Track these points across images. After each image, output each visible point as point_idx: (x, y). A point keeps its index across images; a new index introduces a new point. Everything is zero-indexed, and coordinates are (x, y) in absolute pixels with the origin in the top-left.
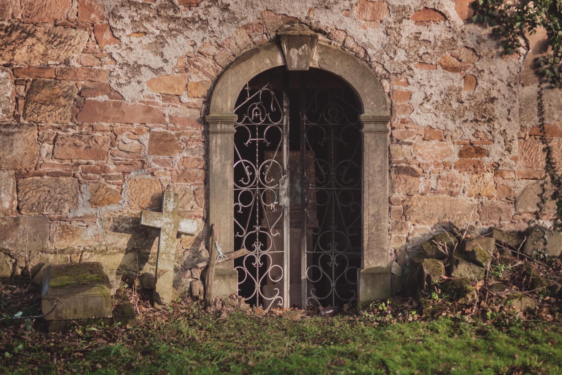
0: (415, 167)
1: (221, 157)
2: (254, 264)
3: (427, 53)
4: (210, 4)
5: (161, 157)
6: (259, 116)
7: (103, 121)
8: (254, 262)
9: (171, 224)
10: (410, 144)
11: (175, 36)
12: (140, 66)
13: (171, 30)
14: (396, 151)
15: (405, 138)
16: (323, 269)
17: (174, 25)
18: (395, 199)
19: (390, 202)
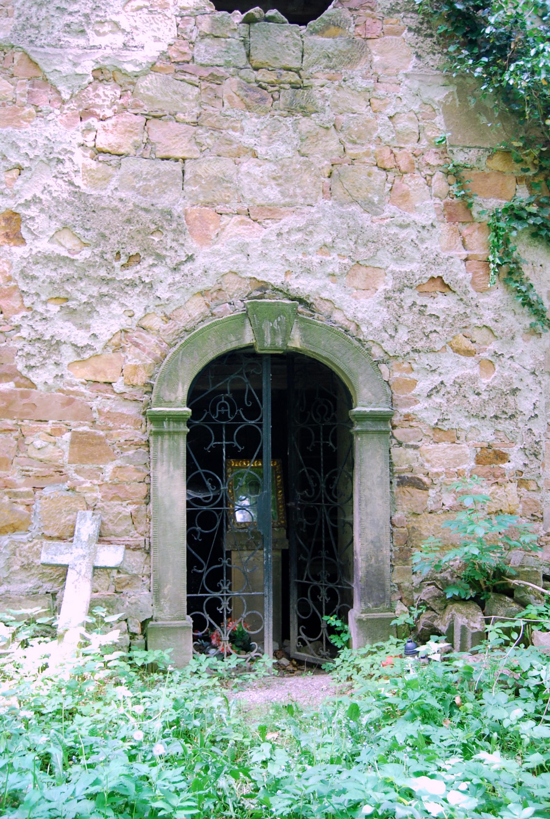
0: (421, 476)
1: (169, 466)
2: (220, 610)
3: (435, 331)
4: (156, 263)
5: (87, 467)
6: (226, 413)
7: (8, 418)
8: (220, 606)
9: (84, 556)
10: (416, 447)
11: (107, 304)
12: (58, 343)
13: (102, 295)
14: (399, 457)
15: (410, 440)
16: (210, 616)
17: (107, 289)
18: (399, 519)
19: (393, 525)
